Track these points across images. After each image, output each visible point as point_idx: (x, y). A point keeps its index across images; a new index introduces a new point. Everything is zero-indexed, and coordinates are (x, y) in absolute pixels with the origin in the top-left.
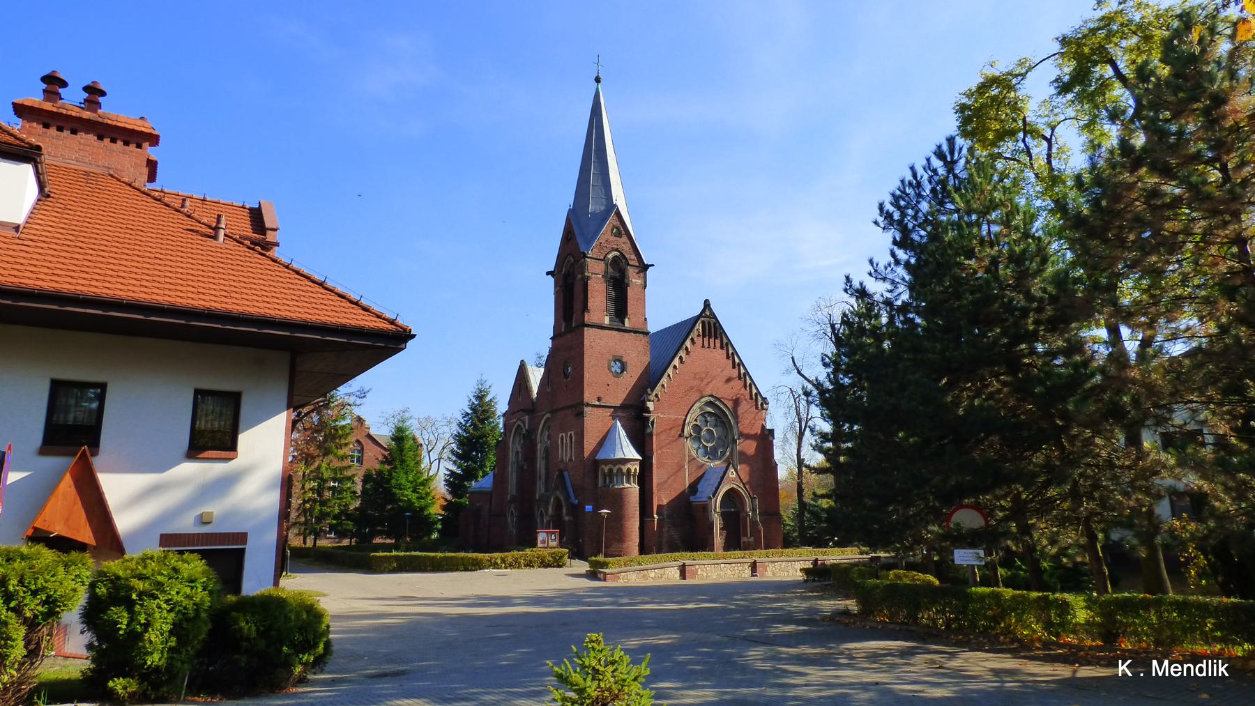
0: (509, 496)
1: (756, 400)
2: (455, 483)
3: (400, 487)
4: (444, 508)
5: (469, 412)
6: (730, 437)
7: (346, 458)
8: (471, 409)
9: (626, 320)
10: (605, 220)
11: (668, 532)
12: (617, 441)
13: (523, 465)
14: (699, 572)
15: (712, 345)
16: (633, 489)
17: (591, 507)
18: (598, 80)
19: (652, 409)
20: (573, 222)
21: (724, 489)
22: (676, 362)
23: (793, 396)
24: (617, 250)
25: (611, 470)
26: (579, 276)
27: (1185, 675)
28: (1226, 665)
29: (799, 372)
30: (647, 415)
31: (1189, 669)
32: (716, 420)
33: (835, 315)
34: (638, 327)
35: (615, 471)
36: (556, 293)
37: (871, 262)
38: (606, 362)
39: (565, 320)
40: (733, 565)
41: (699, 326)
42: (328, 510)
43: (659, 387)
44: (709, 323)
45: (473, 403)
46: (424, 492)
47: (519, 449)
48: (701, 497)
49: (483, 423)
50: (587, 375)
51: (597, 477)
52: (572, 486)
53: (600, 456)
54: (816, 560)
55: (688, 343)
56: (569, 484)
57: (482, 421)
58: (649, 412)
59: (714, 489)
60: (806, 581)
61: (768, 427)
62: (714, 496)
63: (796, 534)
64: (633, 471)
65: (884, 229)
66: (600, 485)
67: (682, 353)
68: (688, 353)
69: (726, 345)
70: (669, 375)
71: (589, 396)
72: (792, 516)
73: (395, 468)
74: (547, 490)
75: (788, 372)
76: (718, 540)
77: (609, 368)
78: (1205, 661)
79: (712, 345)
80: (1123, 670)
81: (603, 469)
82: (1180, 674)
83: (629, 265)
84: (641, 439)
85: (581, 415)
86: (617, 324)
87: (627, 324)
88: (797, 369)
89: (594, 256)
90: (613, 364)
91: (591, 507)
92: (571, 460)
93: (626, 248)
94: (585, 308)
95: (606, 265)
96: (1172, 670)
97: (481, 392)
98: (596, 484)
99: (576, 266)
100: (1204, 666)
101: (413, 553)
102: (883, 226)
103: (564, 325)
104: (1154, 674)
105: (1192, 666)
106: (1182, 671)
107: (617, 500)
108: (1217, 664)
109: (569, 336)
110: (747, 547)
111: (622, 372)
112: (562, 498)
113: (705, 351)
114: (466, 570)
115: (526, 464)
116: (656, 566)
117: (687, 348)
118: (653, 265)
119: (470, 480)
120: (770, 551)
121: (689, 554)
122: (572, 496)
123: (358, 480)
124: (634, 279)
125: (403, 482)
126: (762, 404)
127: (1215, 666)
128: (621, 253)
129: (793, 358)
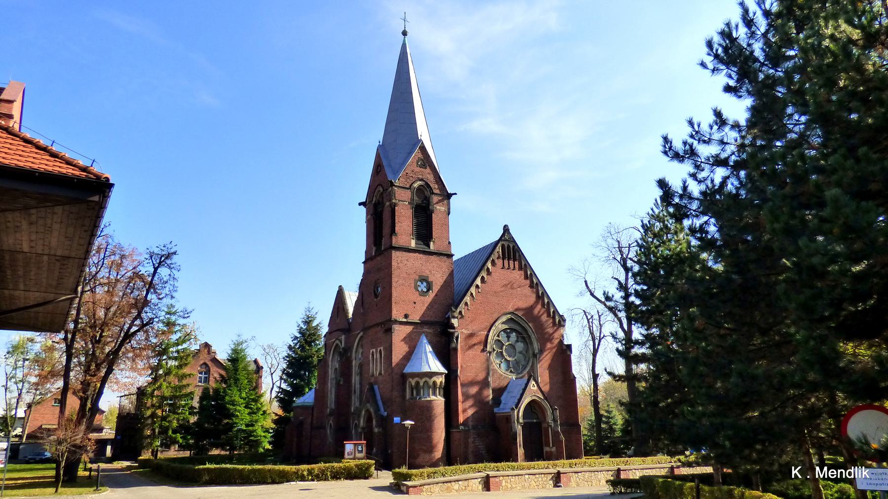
0: (328, 410)
1: (554, 318)
2: (285, 400)
3: (233, 403)
4: (275, 422)
5: (298, 335)
6: (531, 352)
7: (186, 377)
8: (300, 333)
9: (432, 243)
10: (411, 153)
11: (473, 442)
13: (339, 381)
14: (504, 484)
15: (512, 266)
16: (438, 401)
19: (456, 325)
20: (385, 163)
21: (526, 401)
22: (478, 281)
23: (587, 317)
24: (422, 180)
25: (418, 383)
26: (388, 204)
29: (592, 294)
31: (841, 473)
32: (518, 337)
33: (622, 243)
34: (442, 250)
35: (421, 384)
36: (368, 221)
37: (691, 123)
39: (375, 245)
40: (537, 476)
41: (499, 249)
42: (167, 424)
43: (462, 305)
44: (509, 246)
45: (302, 328)
46: (255, 408)
47: (337, 366)
49: (310, 345)
50: (395, 294)
51: (404, 390)
52: (382, 399)
53: (408, 370)
54: (619, 470)
55: (489, 265)
56: (378, 397)
57: (309, 344)
58: (454, 328)
59: (516, 401)
60: (613, 494)
61: (566, 343)
62: (516, 408)
63: (592, 443)
64: (439, 384)
65: (713, 71)
67: (484, 274)
68: (489, 273)
69: (525, 267)
71: (397, 313)
72: (587, 427)
73: (230, 386)
74: (360, 404)
75: (581, 294)
76: (521, 451)
79: (512, 266)
81: (410, 382)
83: (433, 193)
84: (446, 354)
85: (389, 331)
86: (423, 247)
88: (590, 291)
89: (401, 185)
90: (419, 283)
92: (380, 374)
93: (430, 178)
94: (393, 231)
95: (413, 193)
97: (309, 317)
98: (404, 396)
99: (384, 195)
101: (224, 466)
102: (711, 66)
103: (374, 249)
106: (837, 475)
107: (424, 414)
109: (379, 258)
110: (549, 457)
111: (428, 290)
112: (372, 410)
113: (504, 272)
114: (274, 482)
115: (342, 379)
116: (457, 477)
117: (488, 269)
118: (455, 194)
119: (298, 396)
120: (574, 461)
121: (493, 465)
122: (382, 409)
123: (197, 399)
124: (439, 208)
125: (237, 398)
126: (559, 321)
129: (586, 282)
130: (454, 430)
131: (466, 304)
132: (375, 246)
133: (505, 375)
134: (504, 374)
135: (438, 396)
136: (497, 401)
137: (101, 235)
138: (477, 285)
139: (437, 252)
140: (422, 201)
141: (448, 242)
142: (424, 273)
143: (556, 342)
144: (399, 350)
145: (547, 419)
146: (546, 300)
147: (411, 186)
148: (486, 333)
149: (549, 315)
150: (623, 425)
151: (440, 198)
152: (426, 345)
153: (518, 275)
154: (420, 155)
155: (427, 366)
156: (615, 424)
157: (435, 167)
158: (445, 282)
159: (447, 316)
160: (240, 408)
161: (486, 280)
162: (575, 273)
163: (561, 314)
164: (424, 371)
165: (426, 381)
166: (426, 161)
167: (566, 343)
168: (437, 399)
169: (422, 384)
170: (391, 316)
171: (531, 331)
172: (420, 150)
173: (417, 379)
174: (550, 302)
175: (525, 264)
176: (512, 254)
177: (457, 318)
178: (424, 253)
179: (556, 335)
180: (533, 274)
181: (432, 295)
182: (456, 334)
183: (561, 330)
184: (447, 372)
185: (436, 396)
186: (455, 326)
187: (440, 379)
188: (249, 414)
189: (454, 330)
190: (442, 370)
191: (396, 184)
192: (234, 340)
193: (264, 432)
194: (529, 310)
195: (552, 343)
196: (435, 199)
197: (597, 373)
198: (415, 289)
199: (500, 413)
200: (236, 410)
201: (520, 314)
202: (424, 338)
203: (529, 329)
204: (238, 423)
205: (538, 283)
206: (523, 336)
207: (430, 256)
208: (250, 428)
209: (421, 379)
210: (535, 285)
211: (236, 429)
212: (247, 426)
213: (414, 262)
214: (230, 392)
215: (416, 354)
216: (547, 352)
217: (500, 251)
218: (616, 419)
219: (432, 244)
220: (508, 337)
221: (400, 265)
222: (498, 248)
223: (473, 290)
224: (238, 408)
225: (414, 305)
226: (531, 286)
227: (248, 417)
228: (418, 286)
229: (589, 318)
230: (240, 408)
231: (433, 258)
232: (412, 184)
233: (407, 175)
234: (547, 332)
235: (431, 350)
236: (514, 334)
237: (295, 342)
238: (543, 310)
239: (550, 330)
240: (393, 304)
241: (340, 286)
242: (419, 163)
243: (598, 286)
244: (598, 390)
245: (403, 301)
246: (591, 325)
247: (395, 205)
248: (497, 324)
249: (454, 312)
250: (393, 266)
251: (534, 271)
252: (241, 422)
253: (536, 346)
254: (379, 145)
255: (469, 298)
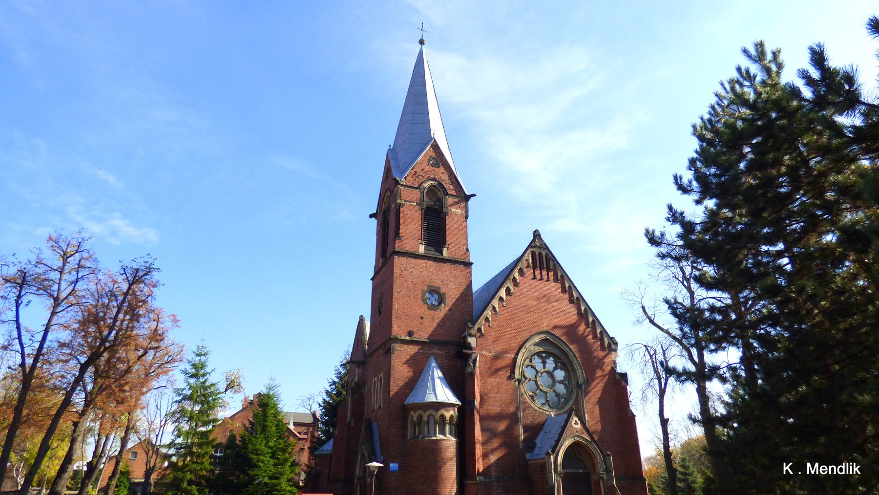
1: (602, 340)
5: (336, 380)
6: (573, 381)
12: (430, 382)
16: (449, 442)
17: (396, 465)
18: (422, 42)
20: (392, 164)
21: (567, 443)
22: (502, 293)
23: (649, 353)
24: (434, 179)
25: (420, 417)
27: (830, 473)
28: (859, 467)
29: (652, 322)
30: (469, 352)
31: (833, 469)
34: (458, 257)
38: (419, 293)
43: (481, 320)
44: (540, 254)
48: (538, 452)
51: (405, 427)
53: (411, 400)
55: (516, 274)
56: (376, 437)
58: (471, 348)
61: (619, 370)
62: (553, 452)
66: (409, 438)
67: (510, 284)
68: (516, 283)
70: (494, 308)
75: (639, 322)
77: (424, 300)
78: (844, 464)
80: (787, 470)
82: (826, 472)
83: (447, 194)
85: (388, 352)
86: (433, 253)
87: (445, 253)
88: (649, 318)
91: (396, 465)
92: (380, 407)
93: (444, 178)
96: (821, 469)
98: (404, 436)
100: (843, 467)
104: (808, 473)
105: (835, 467)
106: (828, 471)
108: (853, 465)
111: (440, 304)
117: (514, 279)
118: (474, 195)
126: (609, 344)
127: (851, 467)
128: (439, 182)
129: (643, 308)
130: (469, 482)
131: (487, 319)
132: (382, 257)
133: (541, 410)
134: (538, 409)
135: (448, 435)
136: (530, 444)
137: (79, 250)
138: (501, 297)
139: (451, 259)
140: (434, 203)
141: (465, 248)
142: (435, 283)
143: (608, 369)
144: (400, 372)
145: (597, 469)
146: (591, 319)
147: (420, 185)
148: (513, 356)
149: (595, 337)
150: (704, 483)
151: (456, 200)
152: (435, 369)
153: (553, 288)
154: (433, 154)
155: (433, 395)
156: (694, 482)
157: (450, 166)
158: (461, 294)
159: (463, 336)
160: (264, 459)
161: (512, 292)
162: (630, 298)
163: (611, 336)
164: (428, 401)
165: (431, 415)
166: (439, 159)
167: (619, 370)
168: (446, 438)
169: (426, 419)
170: (390, 333)
171: (572, 355)
172: (433, 148)
173: (419, 412)
174: (596, 320)
175: (562, 275)
176: (545, 262)
177: (475, 336)
178: (435, 259)
179: (607, 360)
180: (572, 286)
181: (444, 310)
182: (473, 357)
183: (613, 355)
184: (460, 403)
185: (445, 435)
186: (472, 346)
187: (452, 412)
188: (275, 465)
189: (471, 352)
190: (453, 399)
191: (401, 183)
192: (266, 384)
193: (291, 486)
194: (570, 330)
195: (603, 371)
196: (450, 200)
197: (666, 417)
198: (422, 301)
199: (534, 460)
200: (259, 460)
201: (557, 333)
202: (433, 360)
203: (571, 353)
204: (259, 475)
205: (579, 297)
206: (563, 362)
207: (443, 264)
208: (274, 481)
209: (425, 411)
210: (577, 300)
211: (257, 482)
212: (271, 478)
213: (422, 270)
214: (254, 439)
215: (421, 381)
216: (598, 380)
217: (530, 259)
218: (694, 476)
219: (445, 250)
220: (544, 363)
221: (404, 273)
222: (526, 255)
223: (495, 303)
224: (262, 458)
225: (421, 320)
226: (571, 301)
227: (272, 468)
228: (427, 298)
229: (651, 354)
230: (264, 459)
231: (446, 266)
232: (422, 183)
233: (415, 174)
234: (595, 357)
235: (441, 375)
236: (551, 358)
237: (332, 387)
238: (588, 330)
239: (601, 354)
240: (394, 319)
241: (361, 316)
242: (431, 162)
243: (658, 312)
244: (669, 438)
245: (407, 316)
246: (655, 361)
247: (400, 205)
248: (527, 345)
249: (471, 328)
250: (394, 274)
251: (587, 302)
252: (264, 474)
253: (581, 374)
254: (390, 149)
255: (490, 313)
